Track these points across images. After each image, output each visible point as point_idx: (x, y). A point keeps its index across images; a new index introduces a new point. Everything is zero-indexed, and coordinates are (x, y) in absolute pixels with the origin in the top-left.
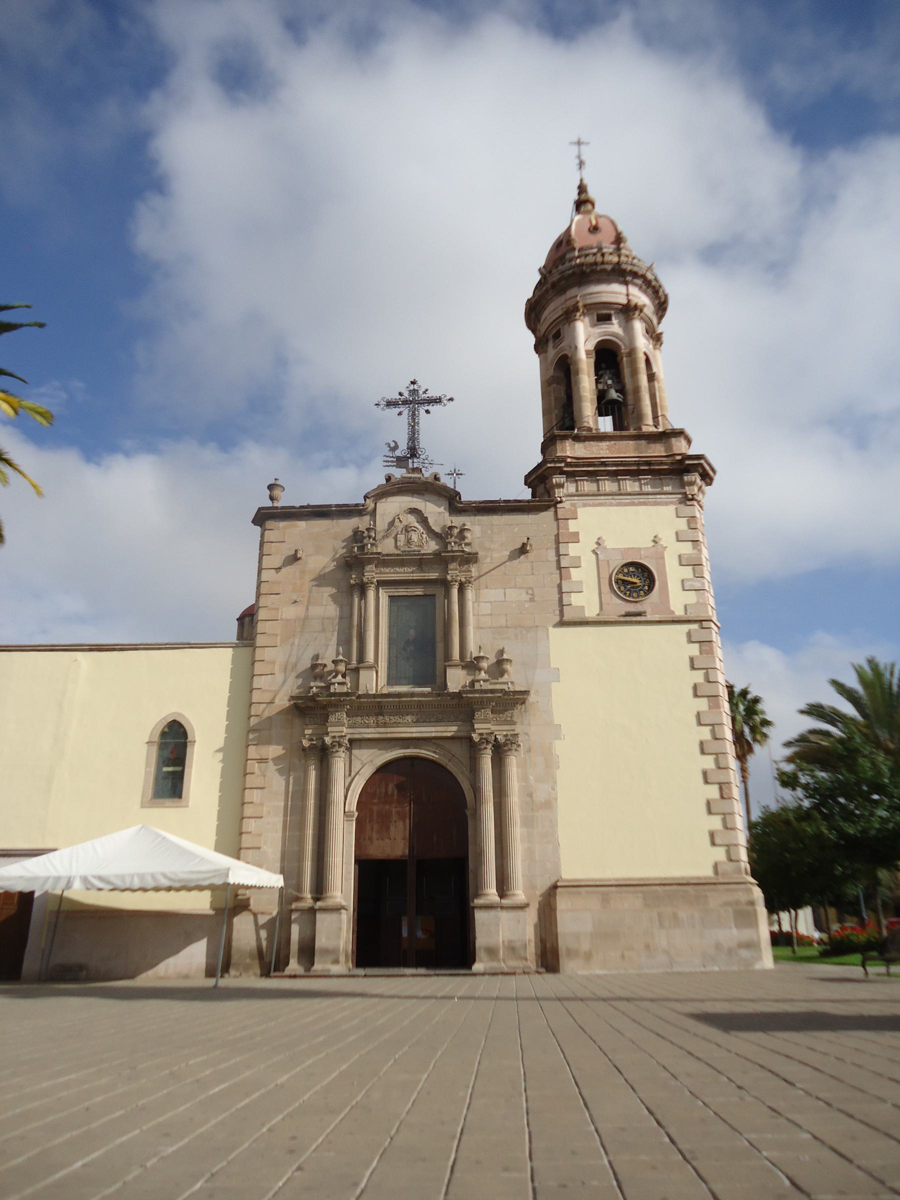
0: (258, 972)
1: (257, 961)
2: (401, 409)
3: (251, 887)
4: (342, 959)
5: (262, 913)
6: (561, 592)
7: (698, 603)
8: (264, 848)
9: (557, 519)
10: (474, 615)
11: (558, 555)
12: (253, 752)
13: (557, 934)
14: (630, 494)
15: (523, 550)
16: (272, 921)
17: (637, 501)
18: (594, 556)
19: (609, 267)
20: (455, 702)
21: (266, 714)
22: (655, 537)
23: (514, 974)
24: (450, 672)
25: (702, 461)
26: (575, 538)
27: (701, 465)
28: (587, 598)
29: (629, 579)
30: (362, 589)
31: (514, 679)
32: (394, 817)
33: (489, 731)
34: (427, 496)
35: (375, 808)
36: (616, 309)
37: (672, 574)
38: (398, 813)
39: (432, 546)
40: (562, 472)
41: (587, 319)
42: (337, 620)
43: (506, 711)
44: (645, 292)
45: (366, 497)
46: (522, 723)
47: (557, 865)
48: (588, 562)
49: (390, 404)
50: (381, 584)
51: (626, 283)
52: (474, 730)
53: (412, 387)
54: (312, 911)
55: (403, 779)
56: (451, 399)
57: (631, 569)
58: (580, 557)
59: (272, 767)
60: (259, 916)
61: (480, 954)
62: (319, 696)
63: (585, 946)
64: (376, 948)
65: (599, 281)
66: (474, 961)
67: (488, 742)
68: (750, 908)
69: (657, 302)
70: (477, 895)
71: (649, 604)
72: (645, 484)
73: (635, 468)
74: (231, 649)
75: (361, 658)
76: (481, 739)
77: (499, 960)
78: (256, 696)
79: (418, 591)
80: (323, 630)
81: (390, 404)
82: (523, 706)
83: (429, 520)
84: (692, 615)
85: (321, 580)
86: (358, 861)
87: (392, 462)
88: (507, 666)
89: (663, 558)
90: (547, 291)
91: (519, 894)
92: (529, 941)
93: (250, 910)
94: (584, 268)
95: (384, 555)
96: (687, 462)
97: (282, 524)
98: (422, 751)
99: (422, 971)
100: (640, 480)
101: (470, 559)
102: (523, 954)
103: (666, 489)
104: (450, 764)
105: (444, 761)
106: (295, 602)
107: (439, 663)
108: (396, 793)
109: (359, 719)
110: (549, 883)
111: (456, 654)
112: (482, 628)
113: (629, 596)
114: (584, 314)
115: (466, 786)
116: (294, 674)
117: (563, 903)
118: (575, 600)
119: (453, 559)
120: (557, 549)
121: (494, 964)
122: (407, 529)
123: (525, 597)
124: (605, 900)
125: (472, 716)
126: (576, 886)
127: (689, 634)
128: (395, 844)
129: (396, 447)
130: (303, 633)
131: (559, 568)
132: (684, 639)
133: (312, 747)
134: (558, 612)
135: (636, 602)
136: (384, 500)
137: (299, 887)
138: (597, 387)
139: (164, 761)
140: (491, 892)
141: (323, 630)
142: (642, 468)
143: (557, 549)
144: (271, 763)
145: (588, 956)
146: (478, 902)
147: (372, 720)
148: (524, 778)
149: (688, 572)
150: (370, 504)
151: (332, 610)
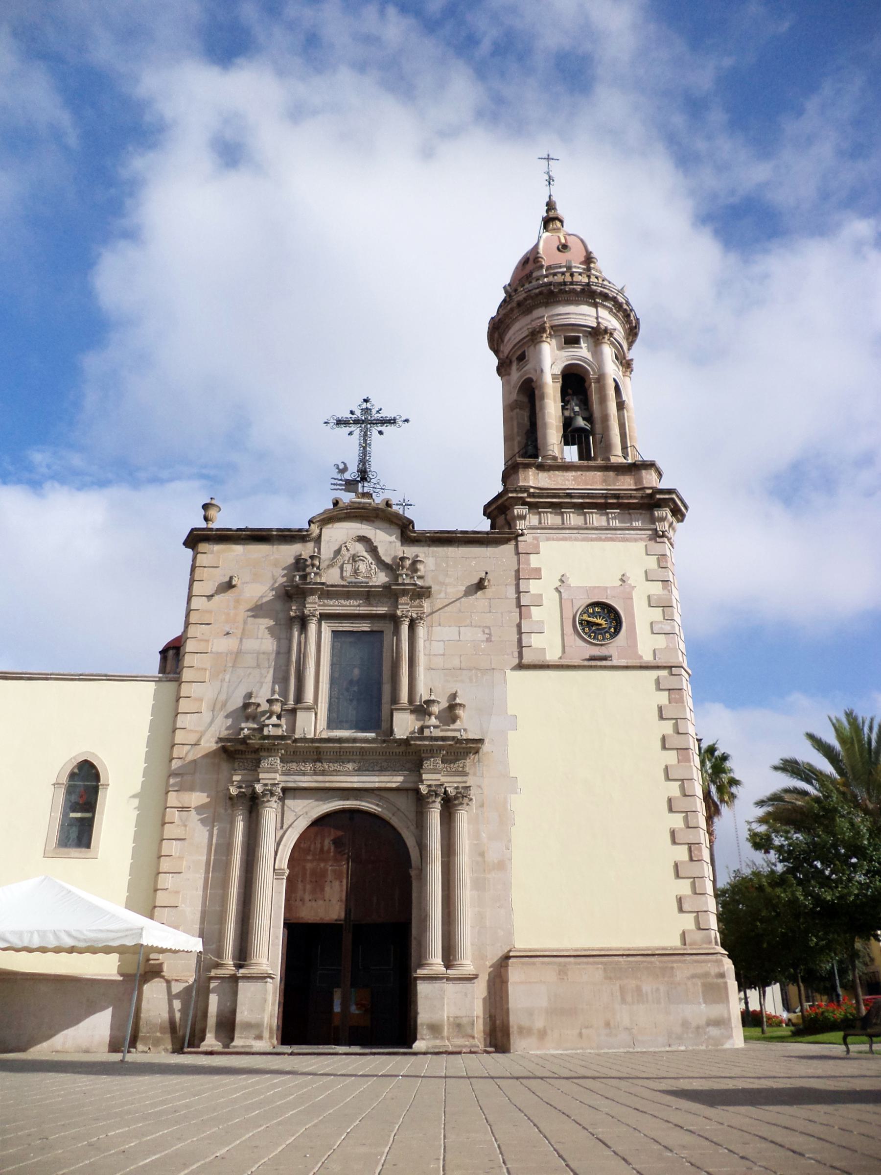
0: (170, 1047)
4: (266, 1034)
5: (177, 980)
6: (520, 633)
8: (182, 906)
9: (518, 553)
11: (518, 592)
12: (173, 799)
13: (508, 1009)
14: (596, 529)
15: (480, 586)
16: (188, 989)
17: (603, 536)
18: (557, 595)
19: (578, 288)
20: (402, 749)
21: (190, 757)
22: (623, 575)
23: (459, 1053)
24: (397, 716)
25: (674, 496)
26: (537, 574)
27: (673, 499)
28: (549, 637)
31: (467, 725)
32: (330, 876)
34: (378, 523)
35: (309, 866)
37: (640, 617)
38: (334, 871)
40: (524, 503)
41: (554, 342)
42: (273, 656)
44: (615, 316)
45: (310, 522)
47: (510, 933)
48: (551, 600)
50: (324, 617)
51: (595, 305)
53: (364, 406)
54: (234, 980)
56: (407, 421)
59: (194, 816)
60: (173, 984)
61: (422, 1031)
62: (250, 739)
63: (539, 1023)
65: (569, 302)
68: (720, 981)
70: (420, 965)
71: (615, 648)
72: (612, 518)
73: (603, 501)
74: (154, 683)
75: (299, 699)
76: (429, 791)
77: (442, 1038)
78: (179, 737)
79: (365, 627)
80: (258, 666)
82: (477, 756)
84: (660, 661)
85: (258, 611)
86: (288, 925)
87: (340, 485)
88: (460, 712)
91: (467, 964)
93: (163, 977)
94: (552, 288)
96: (658, 496)
97: (217, 548)
98: (364, 804)
101: (423, 593)
102: (469, 1031)
103: (636, 524)
105: (387, 815)
106: (228, 633)
108: (332, 850)
109: (294, 766)
110: (500, 954)
113: (594, 638)
117: (515, 974)
118: (535, 641)
119: (404, 592)
120: (518, 586)
122: (354, 558)
124: (562, 972)
127: (658, 681)
128: (329, 906)
130: (235, 666)
131: (519, 606)
133: (241, 796)
134: (516, 654)
135: (602, 645)
136: (330, 526)
137: (220, 954)
140: (436, 962)
141: (258, 666)
142: (610, 501)
143: (518, 586)
144: (193, 812)
145: (542, 1034)
146: (420, 972)
147: (308, 767)
148: (476, 835)
150: (315, 530)
151: (269, 644)
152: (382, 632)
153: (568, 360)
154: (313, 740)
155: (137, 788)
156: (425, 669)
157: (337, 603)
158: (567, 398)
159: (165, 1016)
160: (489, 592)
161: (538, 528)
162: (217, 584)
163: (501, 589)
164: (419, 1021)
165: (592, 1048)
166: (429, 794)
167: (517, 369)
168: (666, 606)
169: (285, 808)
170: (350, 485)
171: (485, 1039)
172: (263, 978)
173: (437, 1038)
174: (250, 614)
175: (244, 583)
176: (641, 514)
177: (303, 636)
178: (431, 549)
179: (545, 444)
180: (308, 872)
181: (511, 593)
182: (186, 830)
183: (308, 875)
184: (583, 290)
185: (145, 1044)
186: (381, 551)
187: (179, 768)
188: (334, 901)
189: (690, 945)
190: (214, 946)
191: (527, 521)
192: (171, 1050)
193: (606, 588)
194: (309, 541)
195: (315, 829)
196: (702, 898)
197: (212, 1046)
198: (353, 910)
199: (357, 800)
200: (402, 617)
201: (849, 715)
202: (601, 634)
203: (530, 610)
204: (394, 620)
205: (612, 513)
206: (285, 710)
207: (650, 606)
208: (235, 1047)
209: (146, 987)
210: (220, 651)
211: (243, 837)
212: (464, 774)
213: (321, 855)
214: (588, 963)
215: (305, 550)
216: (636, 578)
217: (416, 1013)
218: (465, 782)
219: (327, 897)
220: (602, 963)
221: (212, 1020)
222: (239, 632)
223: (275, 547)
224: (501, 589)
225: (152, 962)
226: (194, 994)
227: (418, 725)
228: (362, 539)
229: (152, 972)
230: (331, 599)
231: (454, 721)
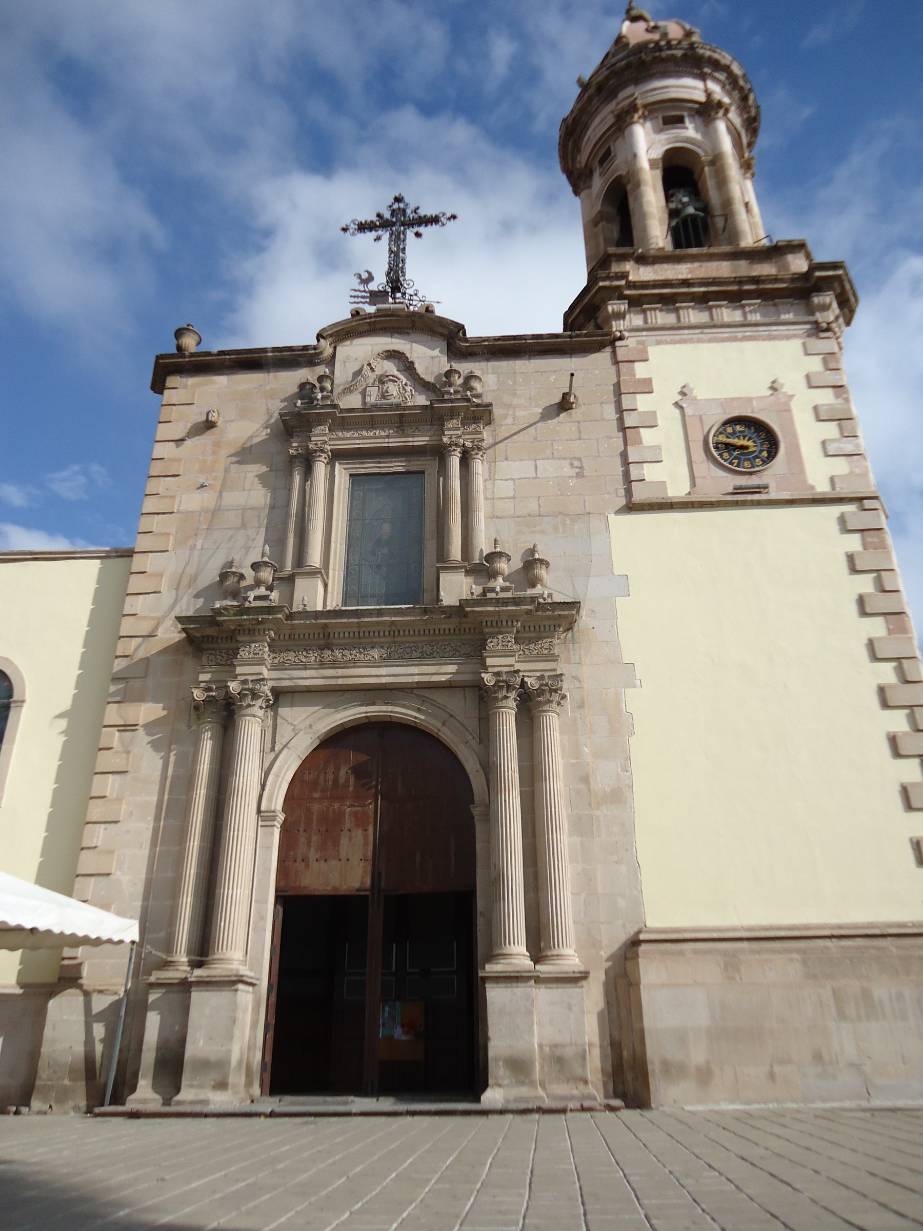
0: (83, 1103)
1: (82, 1084)
2: (380, 232)
3: (98, 942)
4: (237, 1079)
5: (100, 992)
6: (626, 463)
7: (851, 473)
8: (117, 874)
9: (616, 362)
10: (486, 499)
11: (620, 411)
12: (113, 714)
13: (642, 1031)
14: (728, 326)
15: (565, 405)
16: (116, 1005)
17: (740, 335)
18: (677, 412)
19: (678, 53)
20: (453, 623)
21: (141, 654)
22: (774, 382)
23: (563, 1111)
24: (445, 578)
26: (646, 387)
28: (669, 467)
30: (307, 462)
31: (553, 586)
32: (348, 823)
33: (512, 669)
34: (413, 336)
35: (316, 807)
36: (691, 109)
38: (355, 815)
40: (622, 297)
41: (648, 125)
42: (266, 511)
43: (541, 638)
45: (319, 336)
46: (568, 661)
47: (637, 902)
48: (669, 420)
49: (363, 227)
50: (338, 456)
51: (703, 77)
52: (485, 668)
53: (396, 206)
54: (185, 986)
55: (365, 758)
56: (454, 217)
57: (738, 428)
58: (655, 413)
59: (141, 736)
60: (95, 997)
61: (497, 1071)
62: (222, 614)
63: (698, 1056)
64: (314, 1051)
66: (485, 1086)
67: (509, 687)
69: (745, 116)
70: (491, 957)
71: (774, 476)
72: (751, 312)
73: (735, 288)
74: (98, 561)
76: (498, 681)
77: (532, 1084)
78: (127, 627)
79: (398, 466)
80: (244, 526)
81: (363, 227)
82: (570, 634)
83: (416, 365)
84: (844, 490)
85: (245, 455)
86: (282, 899)
87: (363, 297)
88: (541, 572)
89: (789, 411)
90: (590, 100)
91: (569, 956)
92: (591, 1045)
93: (80, 987)
94: (643, 56)
95: (342, 411)
96: (818, 274)
97: (191, 381)
98: (397, 709)
99: (386, 1104)
100: (743, 307)
102: (578, 1071)
103: (784, 317)
104: (444, 729)
106: (202, 486)
107: (429, 573)
108: (352, 780)
109: (291, 656)
110: (623, 936)
111: (455, 551)
112: (498, 517)
113: (738, 466)
114: (644, 117)
115: (471, 764)
116: (192, 591)
117: (651, 972)
120: (618, 403)
121: (524, 1091)
122: (382, 380)
123: (568, 471)
124: (731, 966)
125: (483, 646)
126: (674, 940)
127: (842, 520)
128: (347, 869)
129: (370, 278)
131: (623, 429)
132: (835, 527)
133: (209, 701)
134: (622, 492)
135: (751, 473)
136: (348, 343)
137: (169, 946)
138: (667, 205)
140: (517, 952)
141: (244, 526)
142: (746, 287)
143: (618, 403)
144: (141, 732)
145: (705, 1076)
146: (492, 968)
147: (312, 657)
148: (575, 751)
149: (831, 430)
150: (326, 347)
151: (260, 497)
152: (423, 472)
153: (669, 143)
154: (317, 615)
155: (65, 703)
156: (486, 518)
157: (356, 435)
158: (671, 192)
160: (576, 413)
161: (643, 330)
162: (189, 425)
163: (595, 406)
164: (491, 1053)
165: (793, 1100)
166: (497, 686)
167: (600, 175)
168: (843, 420)
169: (279, 720)
170: (376, 297)
171: (605, 1084)
172: (232, 982)
173: (522, 1083)
174: (234, 459)
175: (226, 422)
176: (792, 304)
177: (309, 483)
178: (491, 364)
179: (644, 229)
180: (315, 817)
181: (610, 412)
182: (128, 760)
183: (315, 822)
184: (685, 55)
185: (44, 1100)
186: (420, 368)
187: (124, 669)
190: (162, 934)
191: (627, 322)
192: (84, 1109)
193: (750, 400)
194: (319, 364)
197: (144, 1101)
198: (384, 874)
199: (387, 704)
200: (450, 445)
202: (748, 460)
203: (639, 433)
205: (750, 305)
206: (280, 579)
207: (819, 420)
208: (180, 1103)
209: (51, 1003)
210: (190, 510)
211: (212, 762)
212: (554, 658)
214: (773, 951)
216: (793, 383)
217: (486, 1039)
218: (555, 670)
219: (343, 856)
220: (798, 951)
221: (148, 1057)
222: (218, 484)
223: (272, 374)
224: (595, 406)
225: (66, 962)
226: (123, 1013)
227: (478, 590)
228: (393, 355)
229: (69, 978)
230: (348, 430)
231: (533, 586)
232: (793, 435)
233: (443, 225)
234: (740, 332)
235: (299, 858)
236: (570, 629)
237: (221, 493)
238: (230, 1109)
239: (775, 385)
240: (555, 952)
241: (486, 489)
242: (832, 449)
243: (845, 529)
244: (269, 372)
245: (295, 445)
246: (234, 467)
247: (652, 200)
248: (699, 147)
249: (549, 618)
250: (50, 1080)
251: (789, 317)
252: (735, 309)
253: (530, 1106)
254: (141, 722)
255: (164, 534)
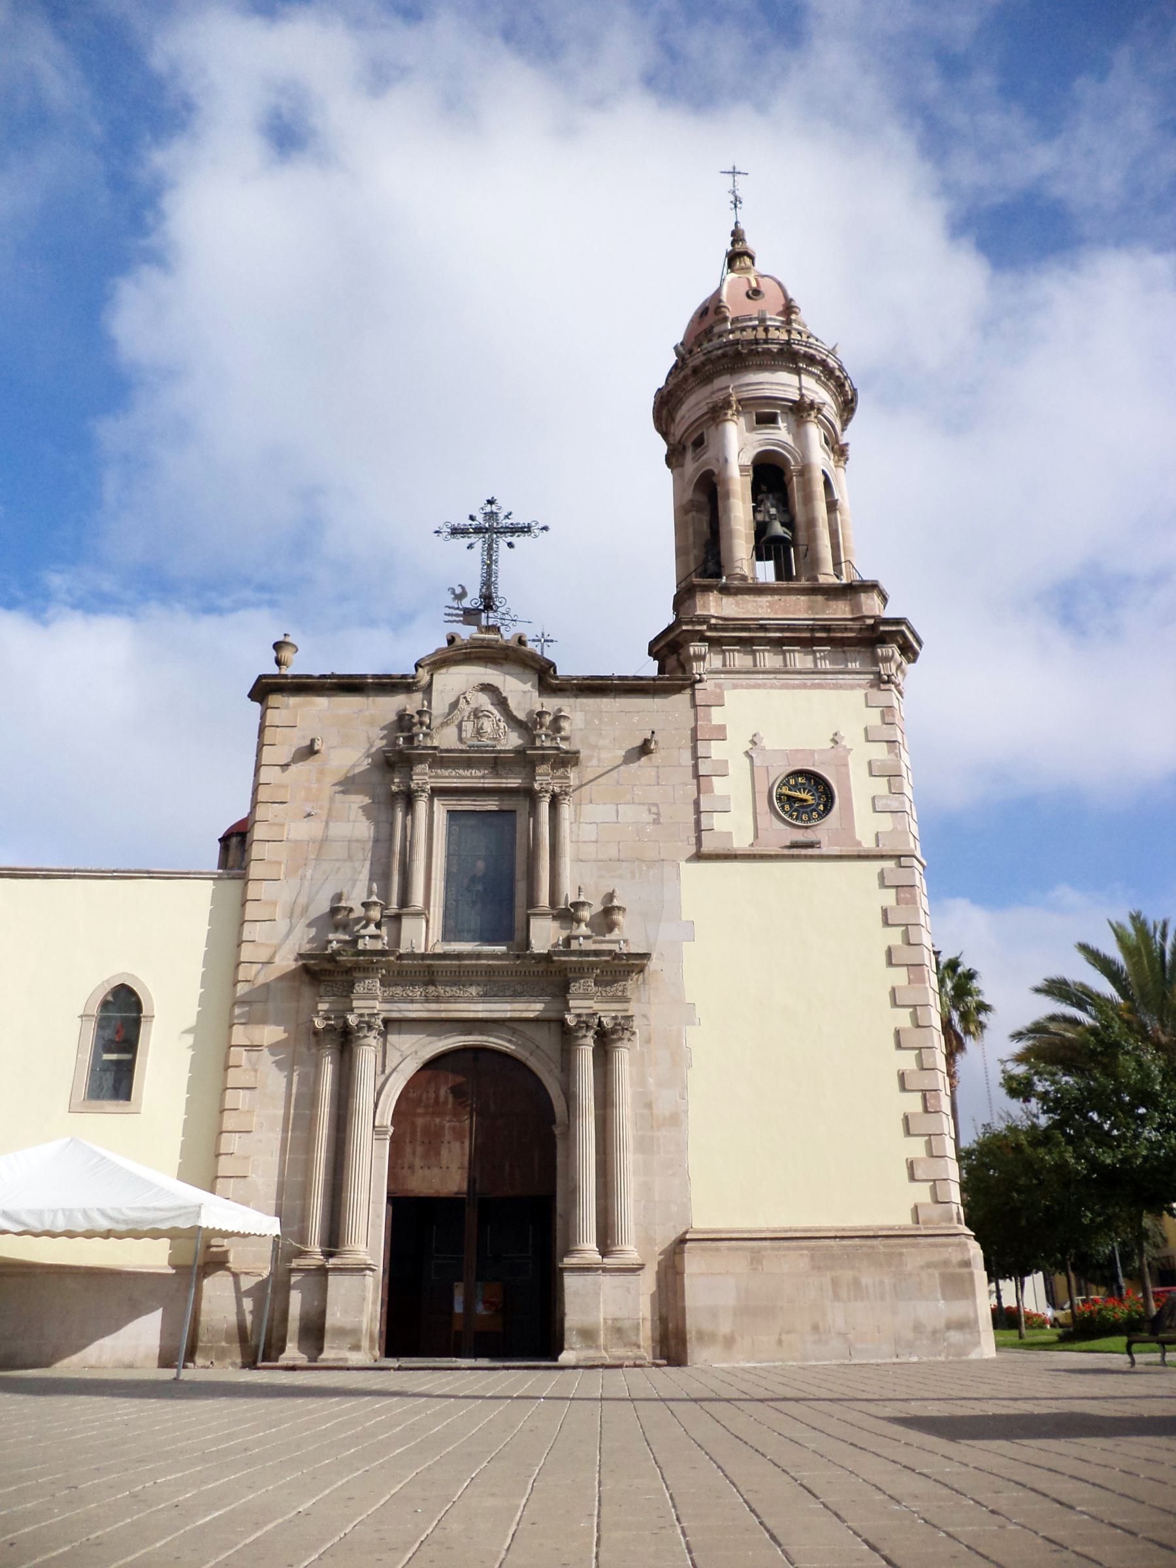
0: (239, 1360)
2: (472, 540)
4: (365, 1343)
5: (247, 1273)
6: (698, 812)
8: (253, 1177)
9: (694, 706)
11: (696, 757)
12: (239, 1034)
13: (684, 1308)
15: (644, 749)
16: (262, 1285)
17: (809, 682)
18: (747, 761)
19: (775, 348)
20: (541, 967)
21: (261, 980)
22: (836, 734)
23: (620, 1366)
24: (535, 923)
25: (904, 628)
26: (720, 733)
27: (902, 633)
28: (737, 817)
29: (797, 794)
30: (409, 799)
31: (629, 935)
32: (448, 1136)
34: (507, 667)
35: (420, 1121)
37: (858, 790)
38: (453, 1129)
39: (512, 740)
40: (703, 639)
41: (742, 420)
42: (371, 844)
43: (616, 981)
44: (825, 385)
46: (639, 1000)
47: (685, 1207)
48: (739, 769)
50: (437, 792)
51: (798, 372)
52: (568, 1010)
53: (488, 509)
54: (323, 1272)
55: (460, 1079)
56: (545, 528)
59: (267, 1058)
61: (571, 1338)
63: (725, 1327)
65: (761, 368)
66: (561, 1349)
68: (965, 1270)
70: (568, 1252)
71: (825, 831)
72: (821, 658)
73: (808, 635)
77: (598, 1347)
78: (246, 953)
79: (491, 805)
80: (350, 858)
83: (510, 702)
84: (885, 848)
85: (348, 784)
86: (393, 1200)
87: (457, 615)
88: (618, 917)
89: (846, 765)
91: (630, 1250)
93: (228, 1269)
94: (740, 347)
96: (882, 628)
98: (491, 1039)
99: (484, 1362)
101: (567, 760)
102: (634, 1339)
105: (522, 1054)
106: (309, 815)
107: (519, 912)
108: (451, 1099)
110: (673, 1236)
113: (797, 819)
114: (738, 412)
115: (554, 1091)
117: (693, 1264)
118: (718, 822)
119: (543, 759)
120: (694, 749)
122: (477, 714)
124: (756, 1260)
127: (881, 875)
128: (447, 1174)
131: (697, 776)
133: (329, 1029)
134: (693, 840)
135: (807, 828)
136: (444, 671)
137: (303, 1237)
139: (105, 1044)
140: (588, 1246)
141: (350, 858)
143: (694, 749)
144: (266, 1052)
146: (568, 1261)
147: (418, 991)
148: (641, 1081)
150: (424, 676)
151: (363, 829)
153: (761, 445)
154: (423, 956)
155: (191, 1020)
156: (572, 861)
158: (759, 497)
159: (233, 1319)
160: (656, 758)
163: (673, 753)
164: (567, 1325)
166: (578, 1027)
170: (470, 616)
171: (654, 1349)
173: (590, 1347)
174: (338, 788)
177: (409, 817)
178: (579, 700)
180: (419, 1130)
181: (686, 758)
183: (419, 1134)
184: (781, 350)
185: (206, 1357)
186: (512, 704)
188: (454, 1168)
189: (924, 1223)
191: (707, 663)
193: (812, 752)
194: (416, 691)
195: (428, 1073)
196: (941, 1161)
200: (541, 791)
201: (1136, 919)
204: (530, 796)
208: (324, 1360)
212: (626, 1000)
213: (436, 1108)
214: (789, 1248)
215: (411, 703)
216: (853, 737)
217: (563, 1315)
218: (626, 1010)
219: (444, 1163)
220: (807, 1248)
221: (293, 1325)
222: (324, 814)
224: (673, 753)
225: (214, 1249)
228: (487, 688)
229: (215, 1262)
232: (847, 789)
233: (536, 536)
234: (810, 679)
235: (406, 1165)
236: (641, 971)
237: (327, 823)
238: (360, 1364)
239: (837, 738)
240: (618, 1248)
241: (571, 832)
242: (880, 805)
243: (883, 885)
244: (368, 696)
245: (396, 780)
246: (339, 797)
247: (740, 513)
248: (789, 453)
249: (623, 965)
250: (210, 1341)
251: (854, 666)
252: (806, 654)
253: (596, 1363)
254: (265, 1044)
255: (276, 862)
